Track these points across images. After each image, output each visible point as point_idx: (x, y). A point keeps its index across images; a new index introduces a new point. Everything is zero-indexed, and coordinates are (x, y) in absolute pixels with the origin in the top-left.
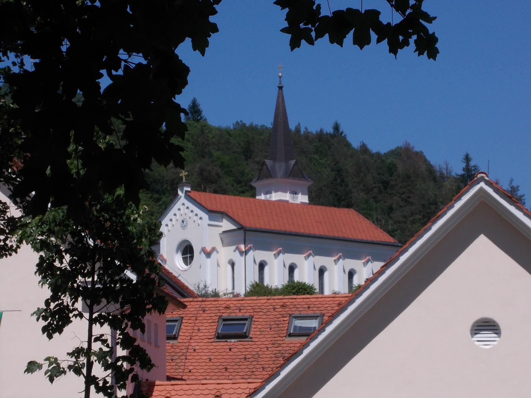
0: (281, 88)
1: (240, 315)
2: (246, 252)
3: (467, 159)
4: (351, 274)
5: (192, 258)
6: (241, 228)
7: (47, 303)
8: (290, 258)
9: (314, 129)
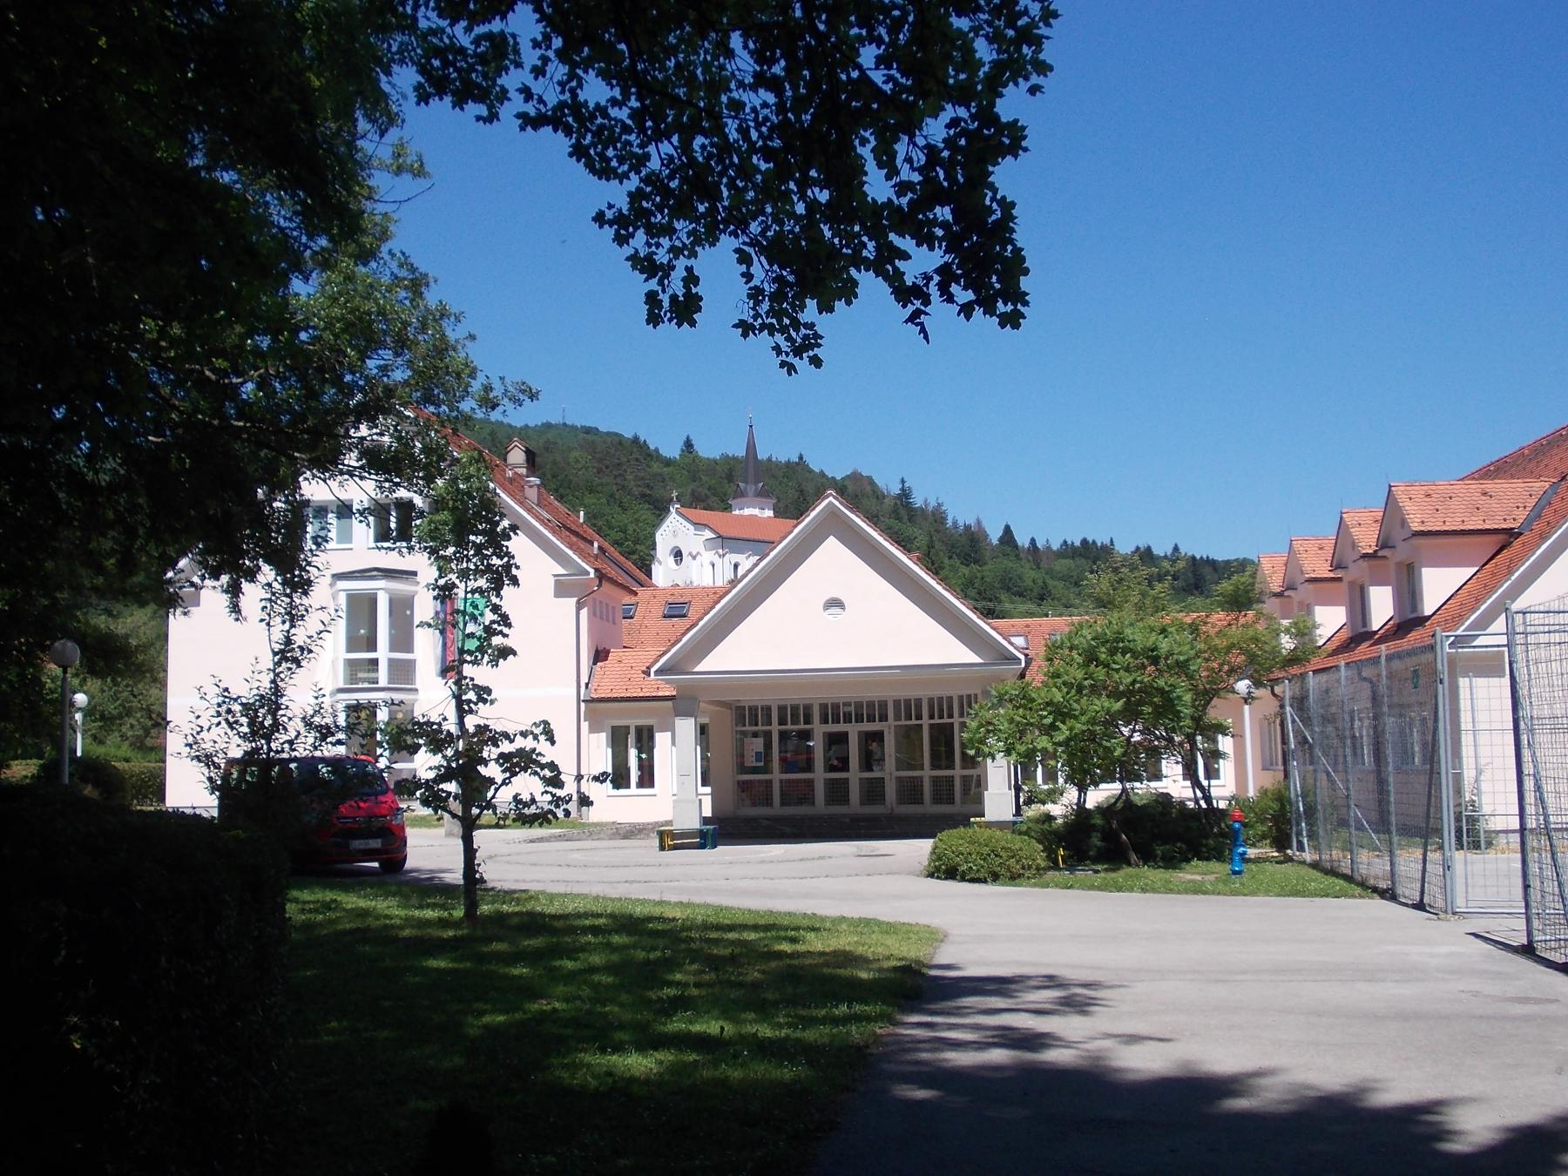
0: (751, 426)
1: (682, 600)
2: (724, 555)
3: (903, 481)
4: (736, 566)
5: (681, 560)
6: (720, 537)
7: (436, 580)
8: (735, 558)
9: (783, 459)
